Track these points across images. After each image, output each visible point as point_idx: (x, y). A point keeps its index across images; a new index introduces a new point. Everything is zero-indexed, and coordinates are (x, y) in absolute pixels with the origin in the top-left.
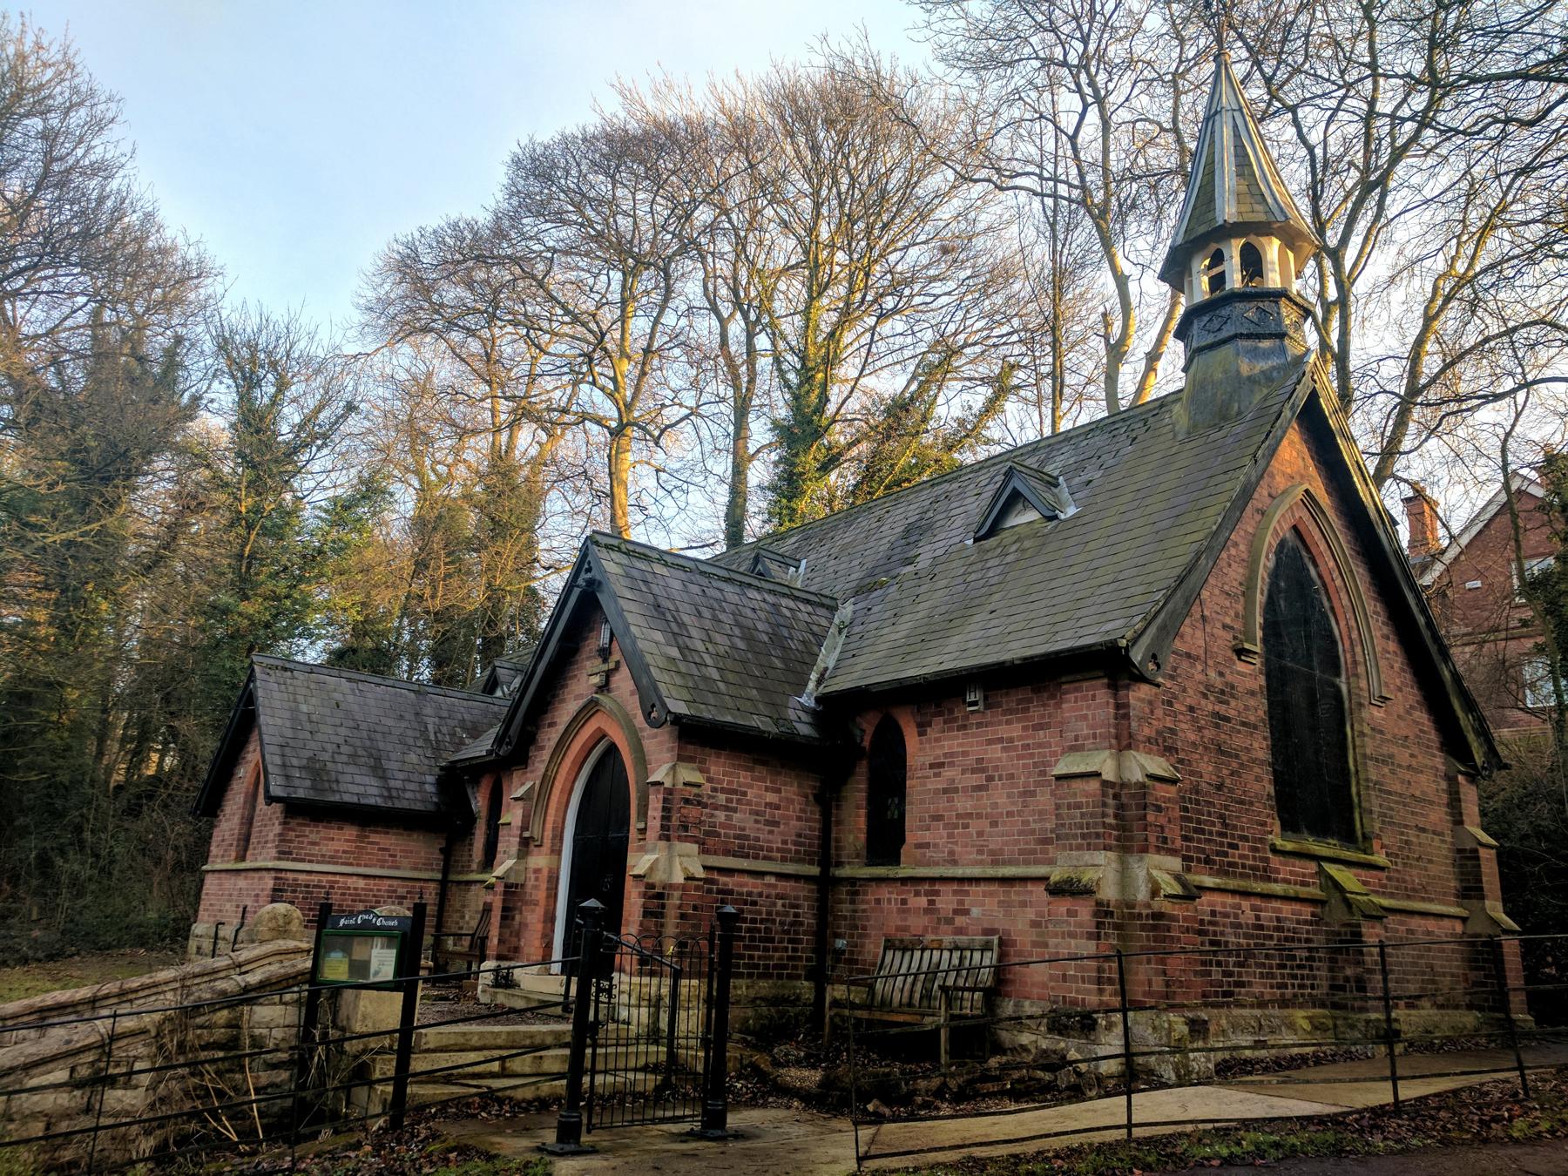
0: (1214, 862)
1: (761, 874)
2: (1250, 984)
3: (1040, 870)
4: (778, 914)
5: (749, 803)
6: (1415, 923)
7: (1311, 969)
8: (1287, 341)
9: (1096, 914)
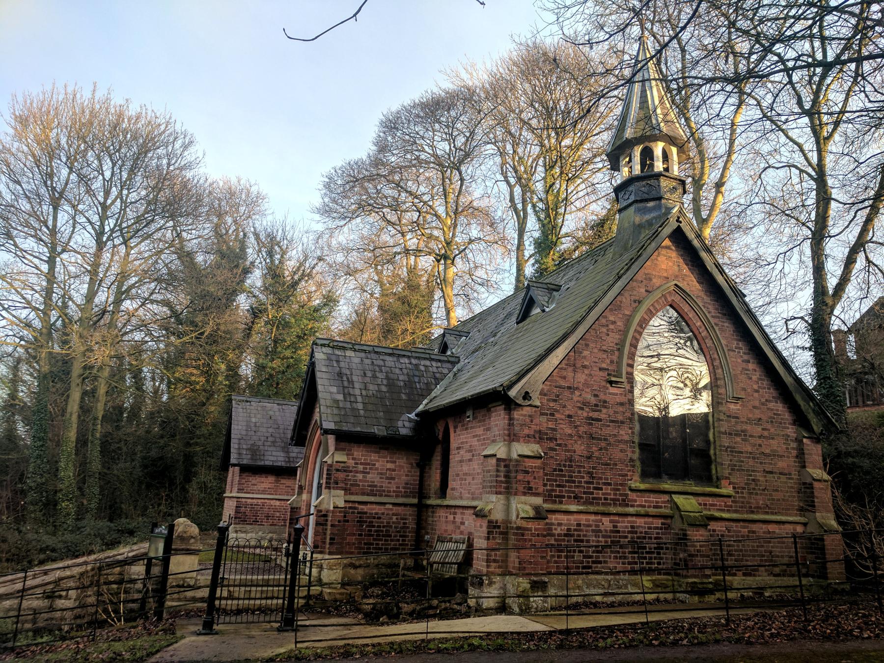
0: (582, 498)
1: (384, 504)
2: (605, 562)
3: (474, 503)
4: (393, 523)
5: (377, 469)
6: (755, 527)
7: (659, 553)
8: (663, 201)
9: (489, 527)
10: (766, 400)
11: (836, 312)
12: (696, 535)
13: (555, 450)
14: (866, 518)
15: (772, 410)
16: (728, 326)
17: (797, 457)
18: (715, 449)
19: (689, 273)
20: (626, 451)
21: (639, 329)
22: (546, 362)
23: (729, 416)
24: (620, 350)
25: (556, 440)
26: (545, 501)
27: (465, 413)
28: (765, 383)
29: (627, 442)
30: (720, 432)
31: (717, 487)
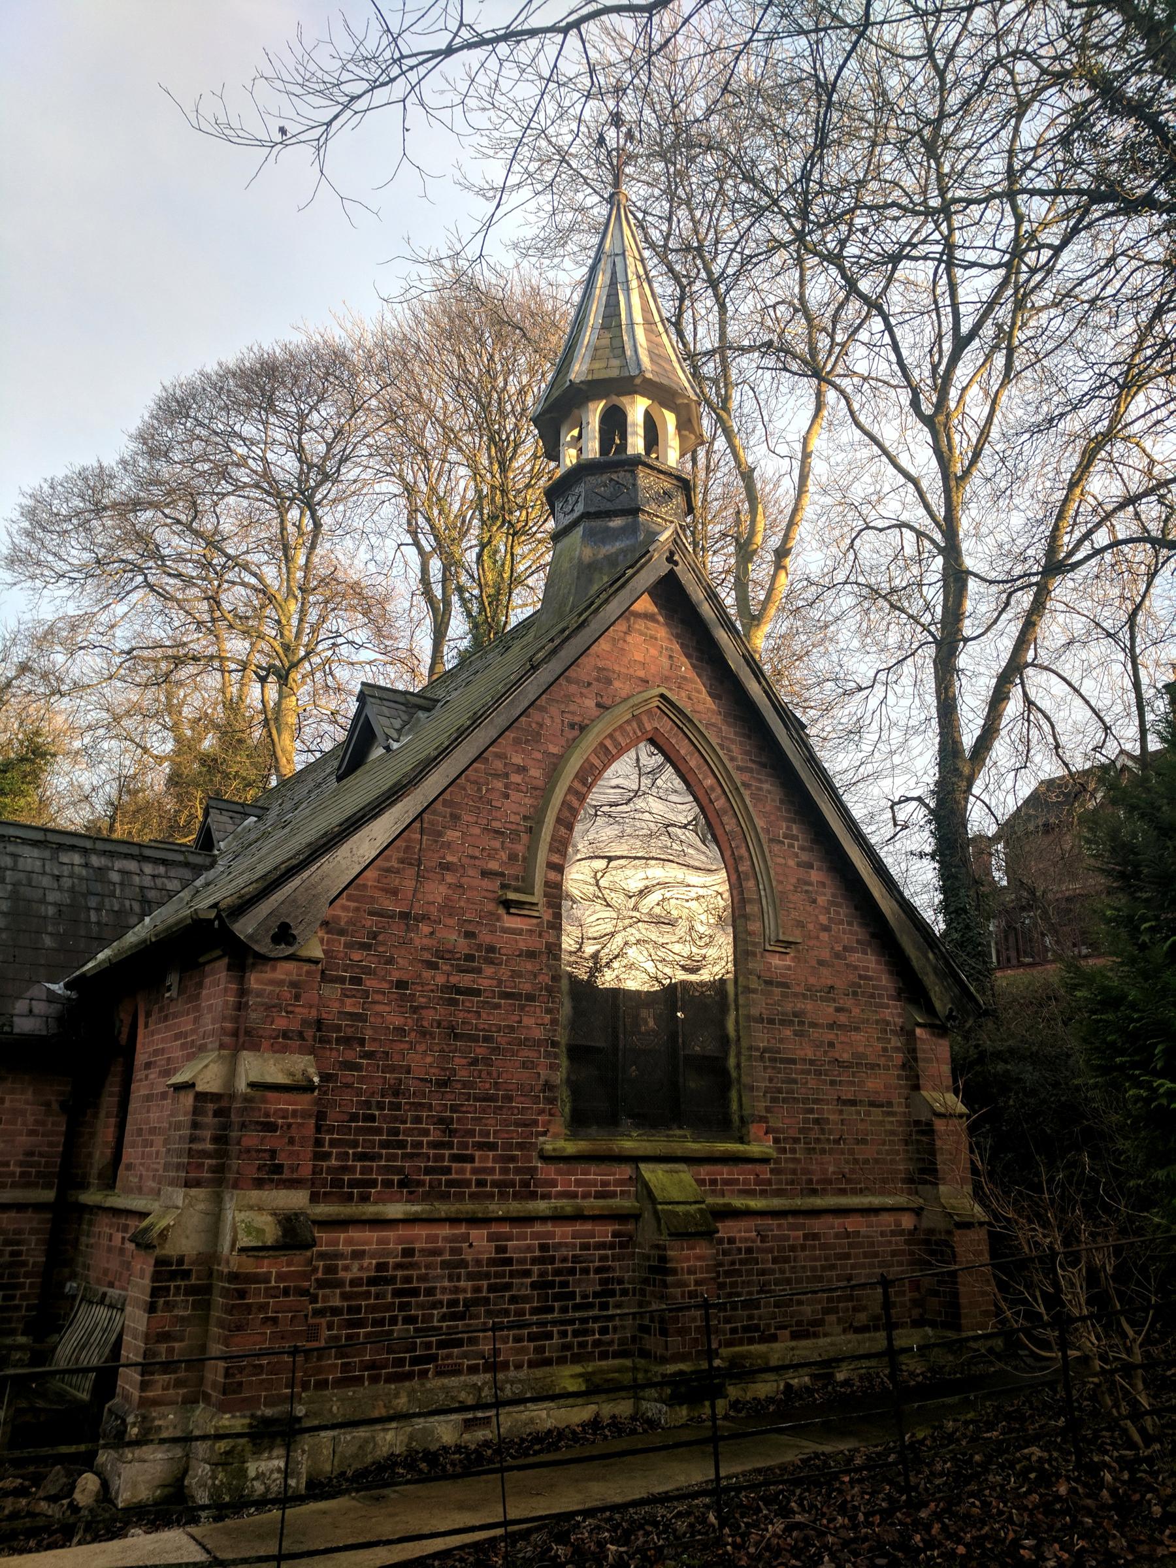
0: (420, 1183)
6: (817, 1225)
8: (642, 518)
9: (156, 1276)
10: (845, 948)
11: (976, 790)
12: (688, 1259)
13: (357, 1067)
14: (1045, 1224)
15: (856, 968)
16: (769, 787)
17: (903, 1066)
18: (738, 1054)
19: (691, 674)
20: (534, 1065)
21: (578, 786)
22: (343, 851)
23: (769, 983)
24: (533, 832)
25: (362, 1042)
26: (314, 1198)
27: (165, 980)
28: (843, 911)
29: (539, 1043)
30: (748, 1018)
31: (741, 1140)
